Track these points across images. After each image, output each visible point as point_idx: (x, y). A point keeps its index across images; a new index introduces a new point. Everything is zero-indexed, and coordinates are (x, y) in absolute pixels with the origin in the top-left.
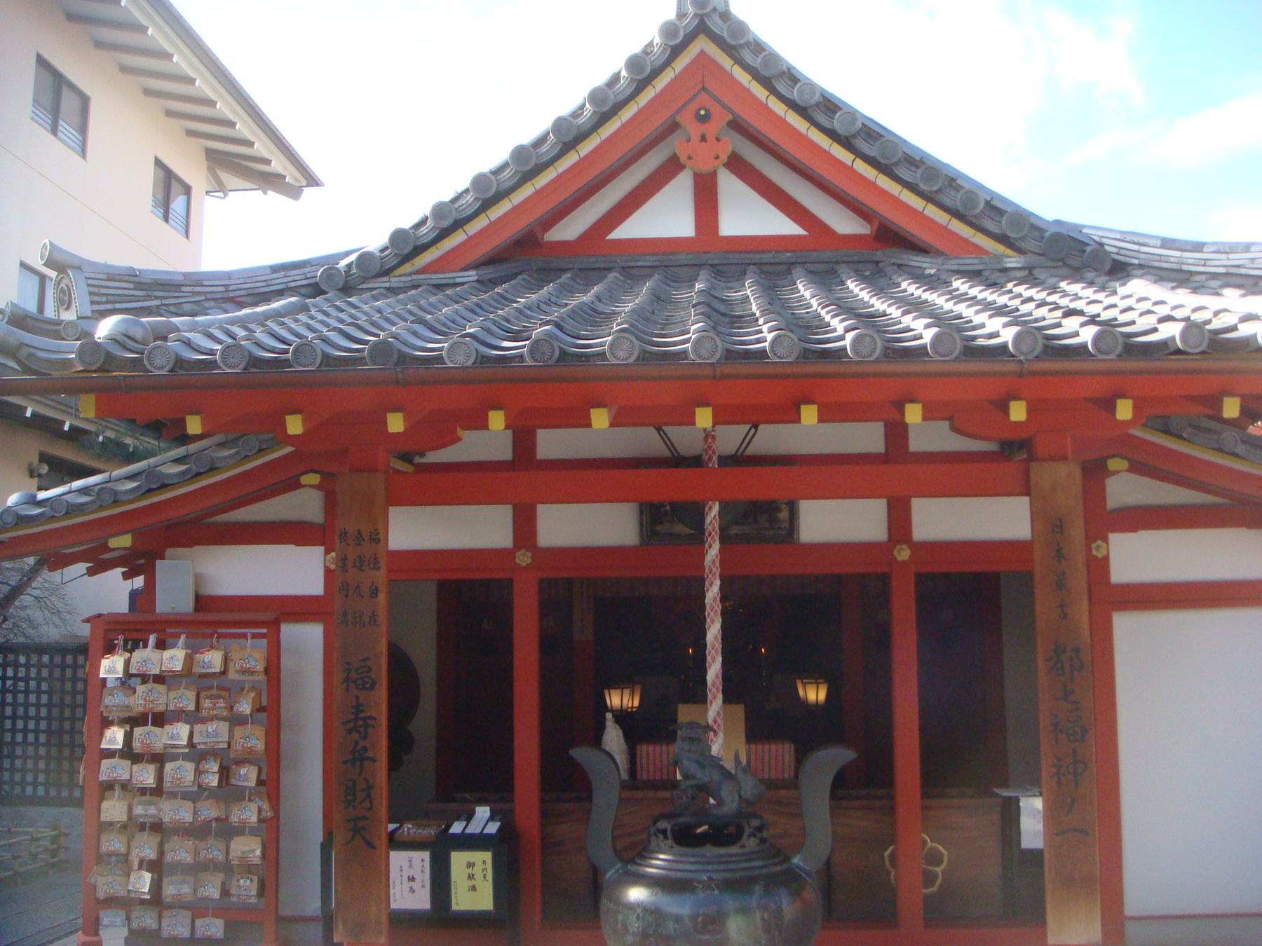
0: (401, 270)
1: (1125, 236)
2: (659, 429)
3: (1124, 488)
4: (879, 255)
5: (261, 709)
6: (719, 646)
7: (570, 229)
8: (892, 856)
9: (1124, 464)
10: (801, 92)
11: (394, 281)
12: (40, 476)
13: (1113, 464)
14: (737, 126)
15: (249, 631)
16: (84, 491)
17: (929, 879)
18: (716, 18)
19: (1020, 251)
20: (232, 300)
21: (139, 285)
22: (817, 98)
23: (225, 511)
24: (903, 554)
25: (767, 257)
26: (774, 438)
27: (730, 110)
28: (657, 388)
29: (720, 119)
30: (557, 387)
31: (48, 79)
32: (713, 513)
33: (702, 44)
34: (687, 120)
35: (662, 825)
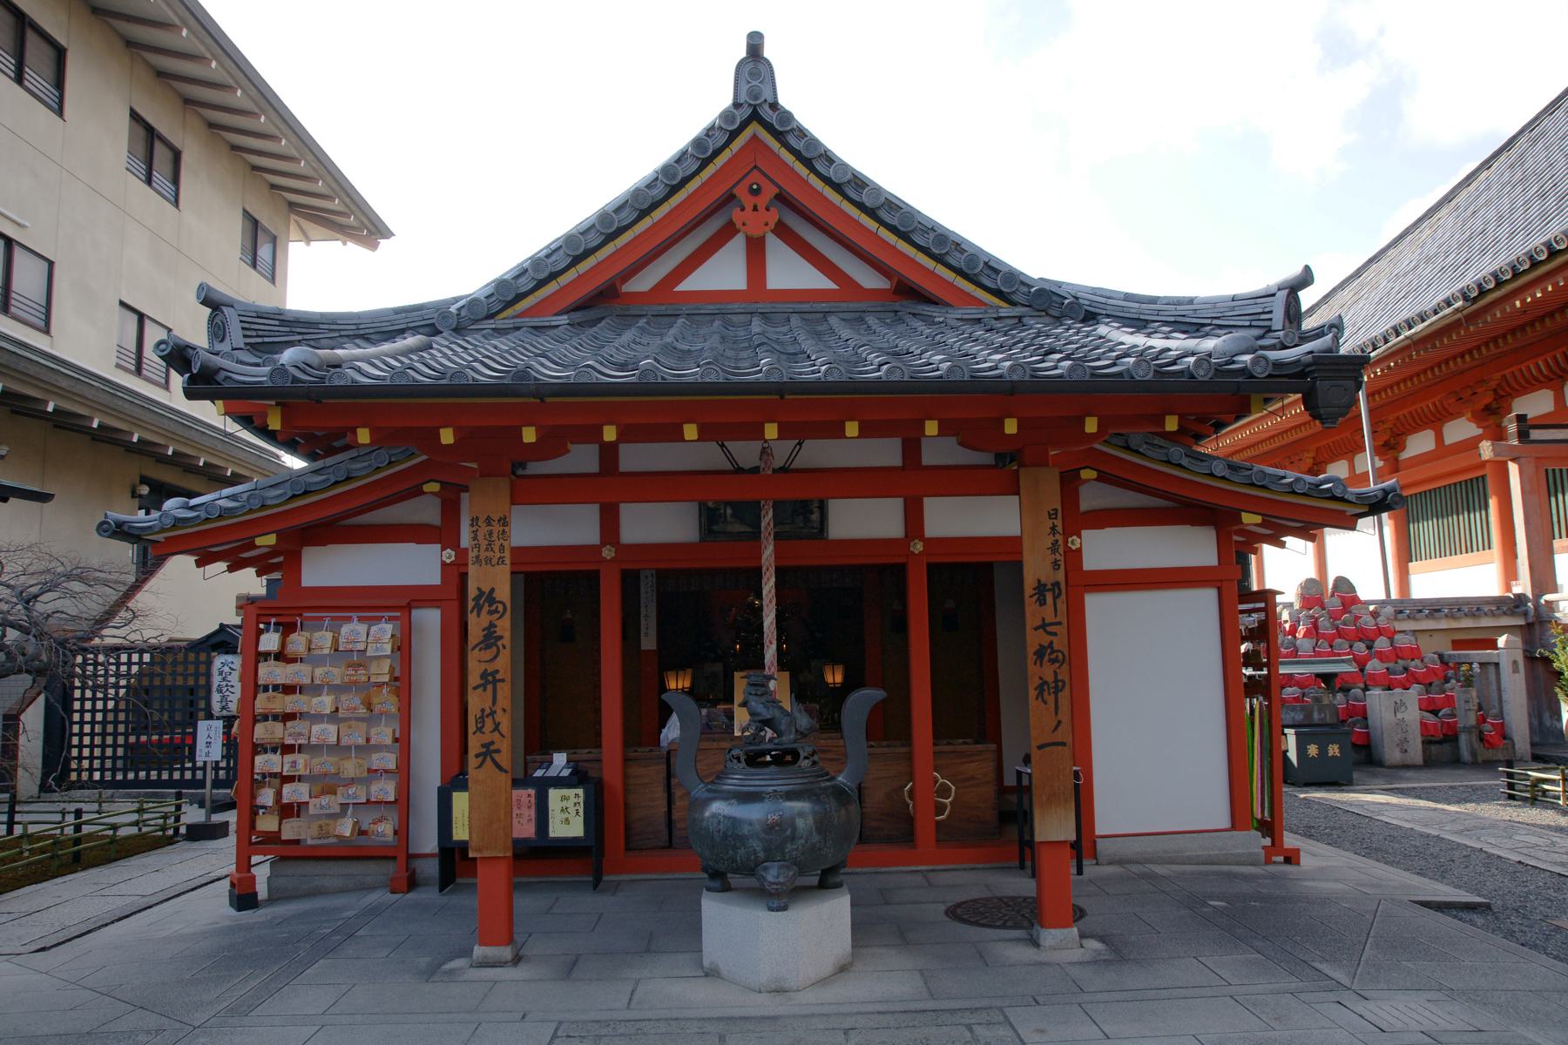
0: (505, 314)
1: (1095, 291)
2: (722, 446)
3: (1093, 496)
4: (897, 306)
5: (396, 679)
6: (766, 642)
7: (644, 282)
8: (911, 791)
9: (1094, 474)
10: (807, 147)
11: (498, 322)
12: (140, 496)
13: (1087, 474)
14: (782, 199)
15: (386, 614)
16: (233, 497)
17: (940, 809)
18: (766, 107)
19: (1013, 304)
20: (362, 337)
21: (284, 323)
22: (849, 176)
23: (360, 513)
24: (918, 547)
25: (806, 307)
26: (820, 453)
27: (777, 185)
28: (729, 409)
29: (770, 192)
30: (653, 409)
31: (142, 132)
32: (767, 518)
33: (754, 128)
34: (741, 192)
35: (735, 752)
